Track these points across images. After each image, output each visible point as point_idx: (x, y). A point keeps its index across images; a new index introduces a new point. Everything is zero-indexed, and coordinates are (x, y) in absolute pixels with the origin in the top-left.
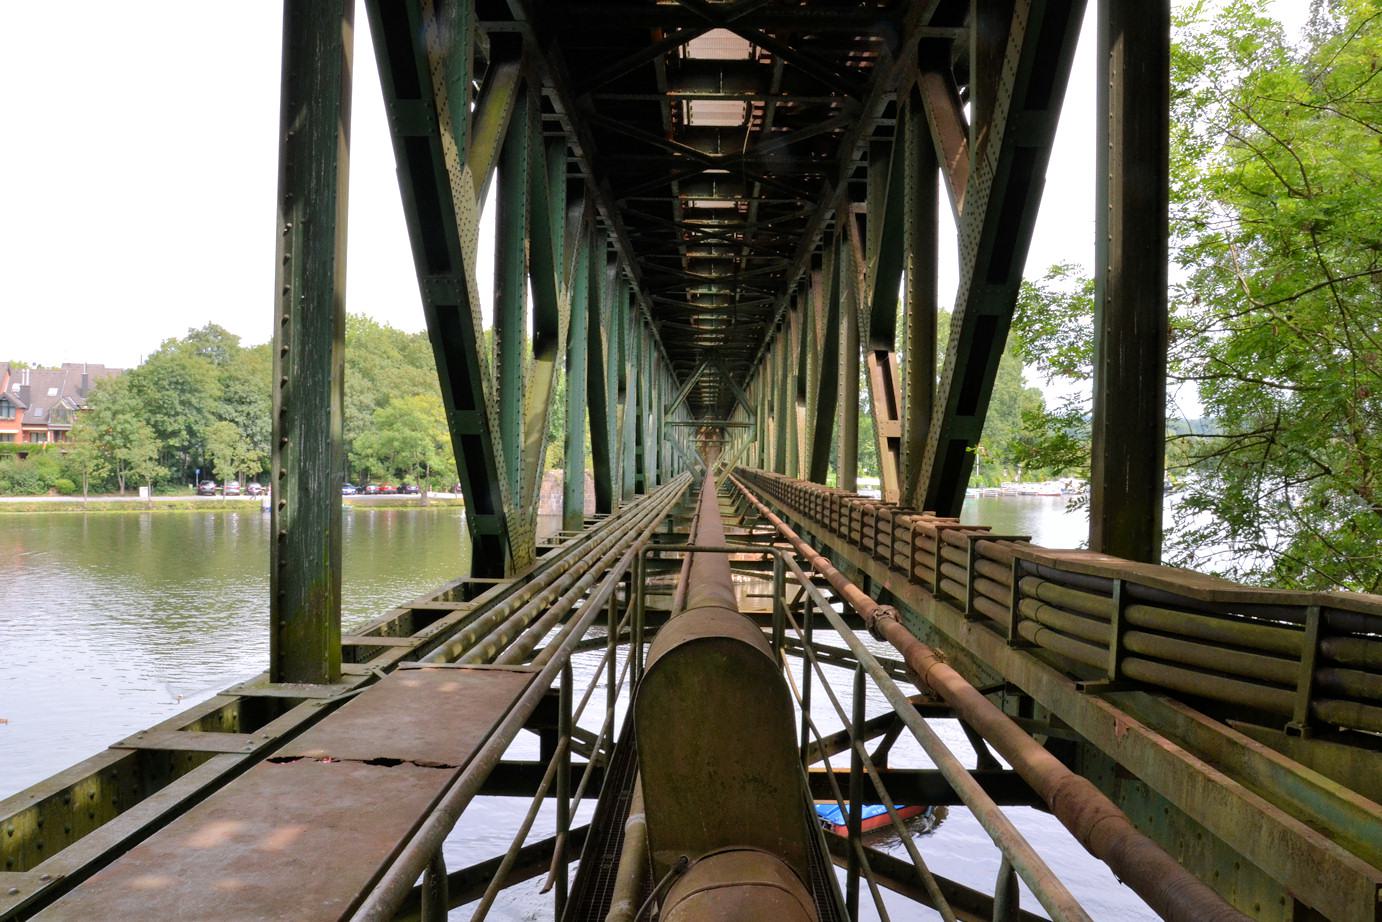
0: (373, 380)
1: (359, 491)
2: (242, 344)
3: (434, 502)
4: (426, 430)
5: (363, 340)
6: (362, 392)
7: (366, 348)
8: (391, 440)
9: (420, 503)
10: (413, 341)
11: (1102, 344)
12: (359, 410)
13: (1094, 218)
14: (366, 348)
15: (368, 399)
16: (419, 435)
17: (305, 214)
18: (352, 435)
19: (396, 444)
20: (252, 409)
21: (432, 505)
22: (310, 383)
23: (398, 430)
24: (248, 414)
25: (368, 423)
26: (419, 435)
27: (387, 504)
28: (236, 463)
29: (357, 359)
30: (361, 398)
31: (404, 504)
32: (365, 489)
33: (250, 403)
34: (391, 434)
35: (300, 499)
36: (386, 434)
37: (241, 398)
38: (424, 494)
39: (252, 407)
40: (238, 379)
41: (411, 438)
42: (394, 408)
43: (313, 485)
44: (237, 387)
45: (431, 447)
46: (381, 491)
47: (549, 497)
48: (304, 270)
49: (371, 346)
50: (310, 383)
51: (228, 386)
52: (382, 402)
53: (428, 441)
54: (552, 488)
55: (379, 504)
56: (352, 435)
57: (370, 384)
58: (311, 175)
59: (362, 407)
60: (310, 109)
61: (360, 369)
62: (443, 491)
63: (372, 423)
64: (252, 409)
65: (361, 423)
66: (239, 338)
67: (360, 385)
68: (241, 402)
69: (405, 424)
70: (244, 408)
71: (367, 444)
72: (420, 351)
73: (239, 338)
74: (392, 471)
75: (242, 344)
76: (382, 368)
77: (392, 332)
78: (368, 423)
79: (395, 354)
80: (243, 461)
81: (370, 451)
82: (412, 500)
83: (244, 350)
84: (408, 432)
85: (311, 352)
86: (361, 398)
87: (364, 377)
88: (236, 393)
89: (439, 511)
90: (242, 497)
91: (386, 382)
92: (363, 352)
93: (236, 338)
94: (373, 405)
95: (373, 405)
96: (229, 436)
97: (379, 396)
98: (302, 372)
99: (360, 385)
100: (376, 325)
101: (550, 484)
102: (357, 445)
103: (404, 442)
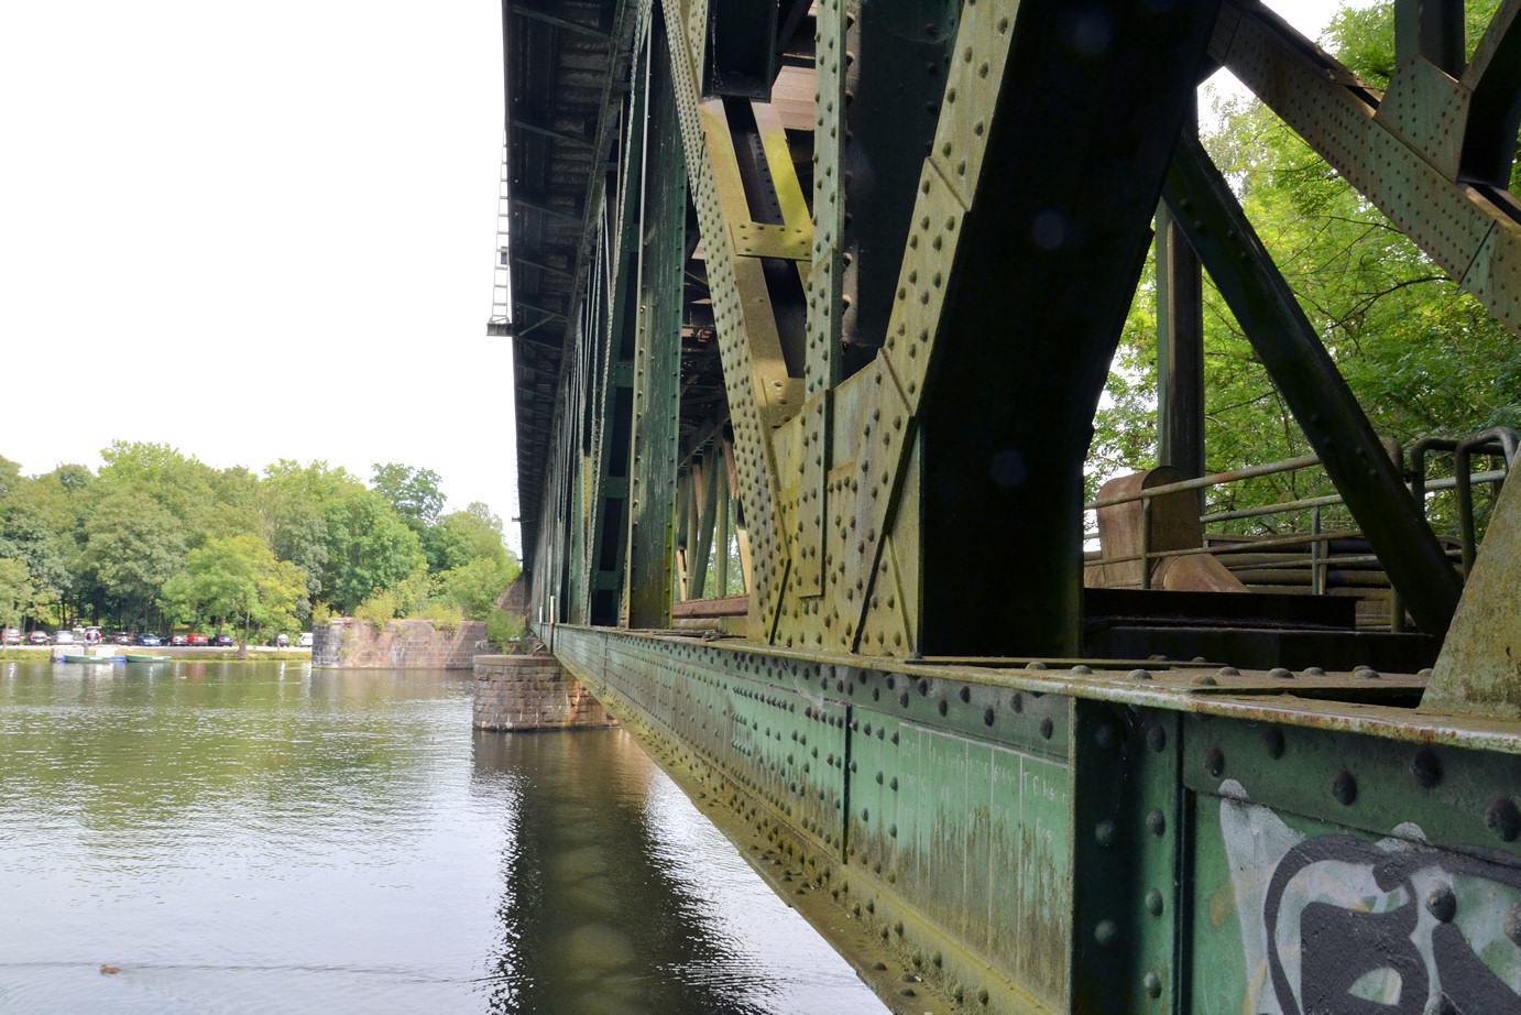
0: (182, 518)
1: (163, 643)
2: (24, 473)
3: (253, 655)
4: (248, 574)
5: (171, 473)
6: (170, 531)
7: (175, 482)
8: (207, 586)
9: (239, 655)
10: (225, 477)
11: (1165, 414)
12: (167, 551)
13: (516, 482)
14: (175, 482)
15: (178, 539)
16: (241, 579)
17: (654, 301)
18: (159, 579)
19: (214, 589)
20: (39, 546)
21: (251, 659)
22: (657, 418)
23: (216, 574)
24: (34, 552)
25: (177, 566)
26: (241, 579)
27: (199, 656)
28: (22, 607)
29: (164, 493)
30: (170, 537)
31: (219, 657)
32: (170, 640)
33: (36, 540)
34: (207, 578)
35: (648, 500)
36: (203, 577)
37: (26, 533)
38: (242, 647)
39: (40, 543)
40: (23, 512)
41: (232, 583)
42: (212, 549)
43: (658, 490)
44: (21, 522)
45: (254, 592)
46: (190, 642)
47: (389, 649)
48: (653, 338)
49: (180, 480)
50: (657, 418)
51: (9, 519)
52: (197, 542)
53: (250, 586)
54: (392, 639)
55: (190, 656)
56: (159, 579)
57: (179, 523)
58: (658, 274)
59: (170, 548)
60: (658, 228)
61: (168, 504)
62: (260, 643)
63: (182, 566)
64: (39, 546)
65: (170, 565)
66: (20, 466)
67: (170, 523)
68: (26, 537)
69: (225, 567)
70: (30, 545)
71: (179, 589)
72: (234, 488)
73: (20, 466)
74: (207, 619)
75: (23, 473)
76: (194, 505)
77: (203, 468)
78: (177, 566)
79: (205, 488)
80: (31, 605)
81: (182, 597)
82: (229, 652)
83: (24, 479)
84: (227, 576)
85: (658, 399)
86: (170, 537)
87: (173, 514)
88: (19, 527)
89: (258, 665)
90: (22, 647)
91: (198, 521)
92: (172, 486)
93: (15, 466)
94: (183, 546)
95: (183, 546)
96: (16, 574)
97: (190, 536)
98: (652, 410)
99: (170, 523)
100: (180, 458)
101: (391, 635)
102: (166, 589)
103: (224, 588)
